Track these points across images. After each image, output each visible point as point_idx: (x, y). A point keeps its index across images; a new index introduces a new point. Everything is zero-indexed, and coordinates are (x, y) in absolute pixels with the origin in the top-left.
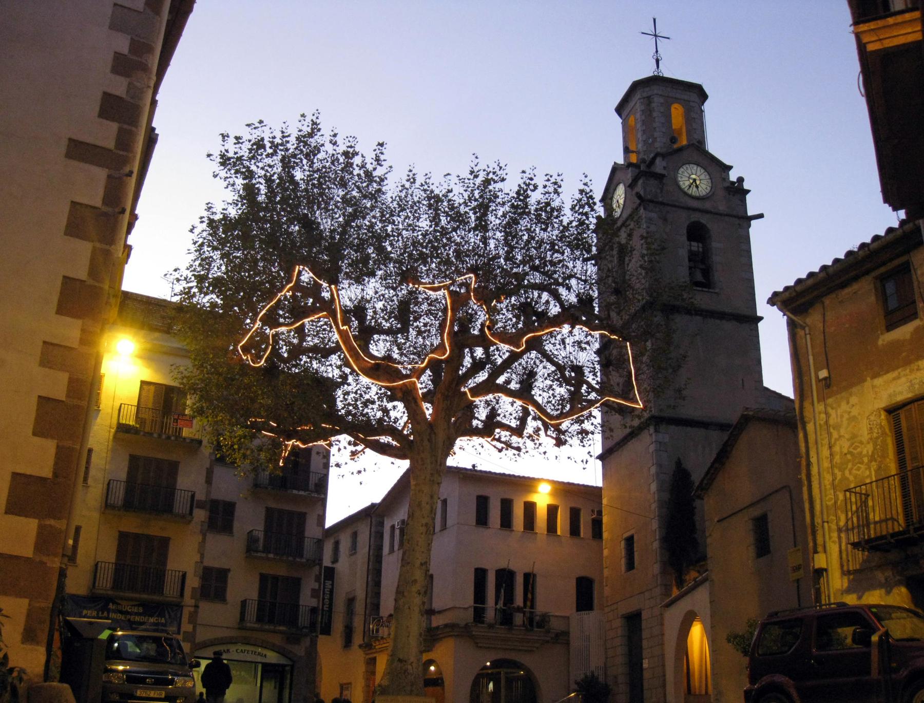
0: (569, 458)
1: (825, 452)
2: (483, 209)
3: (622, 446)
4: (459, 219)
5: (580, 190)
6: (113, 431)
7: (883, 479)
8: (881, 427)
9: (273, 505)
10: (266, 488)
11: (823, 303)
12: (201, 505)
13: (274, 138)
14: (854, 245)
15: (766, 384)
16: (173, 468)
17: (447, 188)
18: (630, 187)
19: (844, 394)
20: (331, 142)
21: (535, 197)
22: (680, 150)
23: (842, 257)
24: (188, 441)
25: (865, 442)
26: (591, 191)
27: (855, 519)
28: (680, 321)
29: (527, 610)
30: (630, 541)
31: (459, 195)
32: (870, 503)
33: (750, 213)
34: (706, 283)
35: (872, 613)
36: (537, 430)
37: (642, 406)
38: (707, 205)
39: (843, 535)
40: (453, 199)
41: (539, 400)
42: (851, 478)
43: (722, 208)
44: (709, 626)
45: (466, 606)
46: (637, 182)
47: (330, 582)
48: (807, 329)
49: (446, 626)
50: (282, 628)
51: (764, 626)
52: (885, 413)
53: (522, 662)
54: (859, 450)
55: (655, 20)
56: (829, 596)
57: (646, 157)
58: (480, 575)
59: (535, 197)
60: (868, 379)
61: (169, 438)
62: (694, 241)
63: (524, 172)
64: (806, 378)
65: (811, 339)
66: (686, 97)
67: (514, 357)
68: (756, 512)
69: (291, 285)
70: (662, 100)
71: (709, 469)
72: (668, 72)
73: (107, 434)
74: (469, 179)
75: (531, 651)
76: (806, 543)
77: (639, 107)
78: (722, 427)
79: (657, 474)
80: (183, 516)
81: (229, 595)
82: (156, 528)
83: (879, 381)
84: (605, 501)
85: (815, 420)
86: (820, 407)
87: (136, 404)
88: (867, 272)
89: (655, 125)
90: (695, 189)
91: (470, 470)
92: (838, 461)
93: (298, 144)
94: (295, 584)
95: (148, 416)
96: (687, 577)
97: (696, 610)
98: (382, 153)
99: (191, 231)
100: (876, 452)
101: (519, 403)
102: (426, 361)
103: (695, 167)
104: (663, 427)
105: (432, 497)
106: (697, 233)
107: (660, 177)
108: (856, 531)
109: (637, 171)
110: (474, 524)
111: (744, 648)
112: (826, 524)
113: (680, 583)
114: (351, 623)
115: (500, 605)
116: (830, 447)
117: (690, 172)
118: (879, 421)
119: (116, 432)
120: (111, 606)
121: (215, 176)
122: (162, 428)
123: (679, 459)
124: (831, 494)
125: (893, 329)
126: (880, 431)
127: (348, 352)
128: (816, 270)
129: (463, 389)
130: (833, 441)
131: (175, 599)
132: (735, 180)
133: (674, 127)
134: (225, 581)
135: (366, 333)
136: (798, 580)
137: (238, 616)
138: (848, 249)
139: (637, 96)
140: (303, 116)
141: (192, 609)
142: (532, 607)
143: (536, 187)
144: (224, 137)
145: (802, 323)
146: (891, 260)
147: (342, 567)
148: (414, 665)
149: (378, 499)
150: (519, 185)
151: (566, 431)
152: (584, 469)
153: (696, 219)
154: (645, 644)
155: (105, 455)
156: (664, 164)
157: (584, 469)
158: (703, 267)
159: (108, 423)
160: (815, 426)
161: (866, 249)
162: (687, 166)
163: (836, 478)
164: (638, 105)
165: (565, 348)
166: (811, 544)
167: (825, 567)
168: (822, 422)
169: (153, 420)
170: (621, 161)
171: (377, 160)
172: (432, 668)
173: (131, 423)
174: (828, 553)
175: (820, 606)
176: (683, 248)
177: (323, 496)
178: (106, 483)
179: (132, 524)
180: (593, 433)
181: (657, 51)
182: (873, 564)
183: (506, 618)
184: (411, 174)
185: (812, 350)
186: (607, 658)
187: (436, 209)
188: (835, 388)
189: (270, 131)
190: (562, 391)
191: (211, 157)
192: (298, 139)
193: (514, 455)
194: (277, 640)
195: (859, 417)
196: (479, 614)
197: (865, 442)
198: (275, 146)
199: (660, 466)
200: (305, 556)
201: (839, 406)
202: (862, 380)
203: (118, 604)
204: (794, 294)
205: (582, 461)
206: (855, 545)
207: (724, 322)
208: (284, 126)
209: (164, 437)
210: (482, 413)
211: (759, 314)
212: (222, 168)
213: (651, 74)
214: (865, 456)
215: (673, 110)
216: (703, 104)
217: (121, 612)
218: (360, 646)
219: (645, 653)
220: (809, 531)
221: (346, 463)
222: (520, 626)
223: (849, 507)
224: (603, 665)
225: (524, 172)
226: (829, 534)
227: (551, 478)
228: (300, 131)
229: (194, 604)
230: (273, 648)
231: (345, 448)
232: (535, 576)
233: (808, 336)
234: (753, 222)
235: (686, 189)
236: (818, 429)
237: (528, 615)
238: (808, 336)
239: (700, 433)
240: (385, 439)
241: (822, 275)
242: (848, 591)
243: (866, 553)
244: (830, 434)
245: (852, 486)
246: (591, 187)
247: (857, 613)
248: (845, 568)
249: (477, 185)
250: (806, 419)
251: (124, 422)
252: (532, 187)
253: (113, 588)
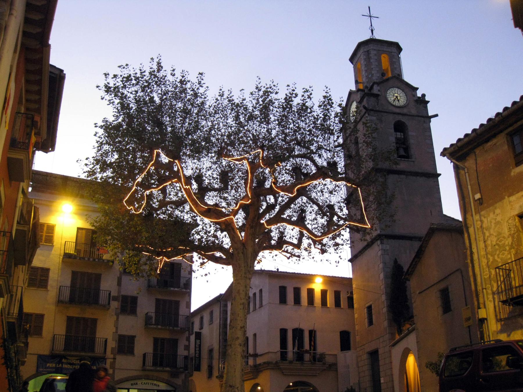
0: (327, 260)
1: (482, 245)
2: (265, 109)
3: (362, 254)
4: (251, 117)
5: (323, 96)
6: (62, 257)
7: (519, 259)
8: (516, 226)
9: (160, 297)
10: (156, 287)
11: (475, 153)
12: (115, 299)
13: (136, 74)
14: (492, 115)
15: (445, 212)
16: (98, 278)
17: (242, 97)
18: (360, 102)
19: (491, 208)
20: (171, 74)
21: (297, 101)
22: (388, 80)
23: (485, 123)
24: (105, 261)
25: (506, 236)
26: (330, 95)
27: (503, 286)
28: (392, 178)
29: (312, 351)
30: (370, 308)
31: (250, 104)
32: (512, 275)
33: (430, 114)
34: (407, 156)
35: (520, 346)
36: (310, 245)
37: (370, 227)
38: (405, 111)
39: (496, 296)
40: (246, 104)
41: (309, 226)
42: (499, 260)
43: (414, 112)
44: (417, 358)
45: (276, 351)
46: (363, 100)
47: (199, 341)
48: (466, 169)
49: (264, 363)
50: (168, 369)
51: (448, 357)
52: (518, 218)
53: (311, 383)
54: (503, 242)
55: (369, 8)
56: (489, 336)
57: (368, 85)
58: (283, 332)
59: (297, 101)
60: (506, 197)
61: (94, 260)
62: (399, 132)
63: (288, 86)
64: (467, 200)
65: (469, 175)
66: (390, 50)
67: (292, 200)
68: (442, 286)
69: (153, 162)
70: (375, 52)
71: (412, 262)
72: (378, 36)
73: (59, 260)
74: (255, 92)
75: (315, 376)
76: (473, 304)
77: (362, 57)
78: (419, 239)
79: (383, 268)
80: (104, 306)
81: (136, 351)
82: (89, 313)
83: (513, 198)
84: (354, 286)
85: (474, 225)
86: (477, 217)
87: (75, 241)
88: (501, 131)
89: (372, 67)
90: (397, 102)
91: (275, 271)
92: (490, 250)
93: (151, 76)
94: (174, 343)
95: (82, 248)
96: (404, 328)
97: (410, 347)
98: (202, 79)
99: (95, 135)
100: (514, 243)
101: (297, 229)
102: (238, 205)
103: (397, 89)
105: (246, 287)
106: (399, 127)
107: (377, 96)
108: (504, 293)
109: (363, 93)
110: (278, 302)
111: (437, 371)
112: (484, 290)
113: (400, 332)
114: (212, 363)
115: (296, 349)
116: (485, 242)
117: (394, 93)
118: (514, 223)
119: (63, 258)
120: (64, 360)
121: (102, 99)
122: (90, 255)
123: (396, 259)
124: (486, 271)
125: (519, 166)
126: (516, 230)
127: (191, 202)
128: (470, 132)
129: (262, 222)
130: (486, 237)
131: (101, 355)
132: (420, 96)
133: (383, 68)
134: (133, 343)
135: (203, 190)
136: (469, 327)
137: (142, 363)
138: (489, 117)
139: (362, 50)
140: (152, 59)
141: (112, 360)
142: (315, 350)
143: (296, 95)
144: (106, 75)
145: (462, 166)
146: (516, 122)
147: (205, 331)
148: (239, 388)
149: (223, 292)
150: (286, 94)
151: (326, 244)
152: (337, 266)
154: (381, 369)
155: (57, 272)
156: (379, 88)
157: (337, 266)
158: (405, 146)
159: (58, 253)
160: (474, 229)
161: (500, 116)
162: (392, 89)
163: (489, 261)
164: (362, 57)
165: (323, 195)
166: (476, 303)
167: (486, 317)
168: (479, 227)
169: (84, 250)
170: (354, 89)
171: (199, 83)
172: (259, 388)
173: (72, 252)
174: (487, 309)
175: (484, 343)
176: (392, 137)
177: (188, 291)
178: (59, 288)
179: (75, 312)
180: (343, 245)
181: (371, 25)
182: (516, 314)
183: (299, 357)
184: (221, 92)
185: (470, 182)
186: (359, 378)
187: (238, 112)
188: (486, 205)
189: (133, 70)
190: (322, 221)
191: (99, 88)
192: (150, 73)
193: (297, 260)
194: (165, 376)
195: (502, 222)
196: (283, 355)
197: (506, 236)
198: (137, 79)
199: (385, 263)
200: (179, 326)
201: (489, 215)
202: (502, 199)
203: (68, 359)
204: (457, 148)
205: (336, 262)
206: (504, 302)
207: (418, 177)
208: (141, 66)
209: (91, 259)
210: (275, 235)
211: (438, 172)
212: (106, 93)
213: (369, 38)
214: (507, 245)
215: (382, 58)
216: (399, 54)
217: (71, 364)
218: (217, 377)
219: (382, 374)
220: (474, 295)
221: (198, 270)
222: (308, 361)
223: (499, 279)
224: (358, 382)
225: (288, 86)
226: (487, 296)
227: (322, 274)
228: (151, 68)
229: (113, 357)
230: (162, 381)
231: (197, 261)
232: (315, 331)
233: (467, 174)
234: (432, 120)
235: (392, 102)
236: (476, 230)
237: (312, 354)
238: (467, 174)
239: (408, 242)
240: (218, 254)
241: (473, 134)
242: (501, 331)
243: (511, 307)
244: (484, 234)
245: (500, 265)
246: (330, 93)
247: (510, 346)
248: (498, 317)
249: (260, 95)
250: (469, 225)
251: (67, 252)
252: (294, 95)
253: (65, 350)
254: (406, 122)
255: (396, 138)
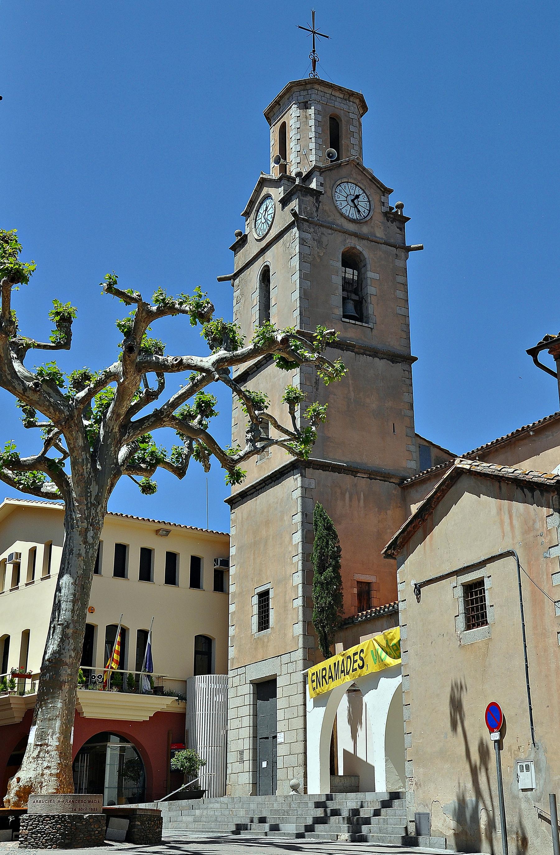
5: (212, 413)
38: (365, 230)
43: (380, 234)
104: (309, 471)
153: (352, 245)
158: (356, 298)
219: (280, 726)
254: (364, 253)
255: (344, 278)
